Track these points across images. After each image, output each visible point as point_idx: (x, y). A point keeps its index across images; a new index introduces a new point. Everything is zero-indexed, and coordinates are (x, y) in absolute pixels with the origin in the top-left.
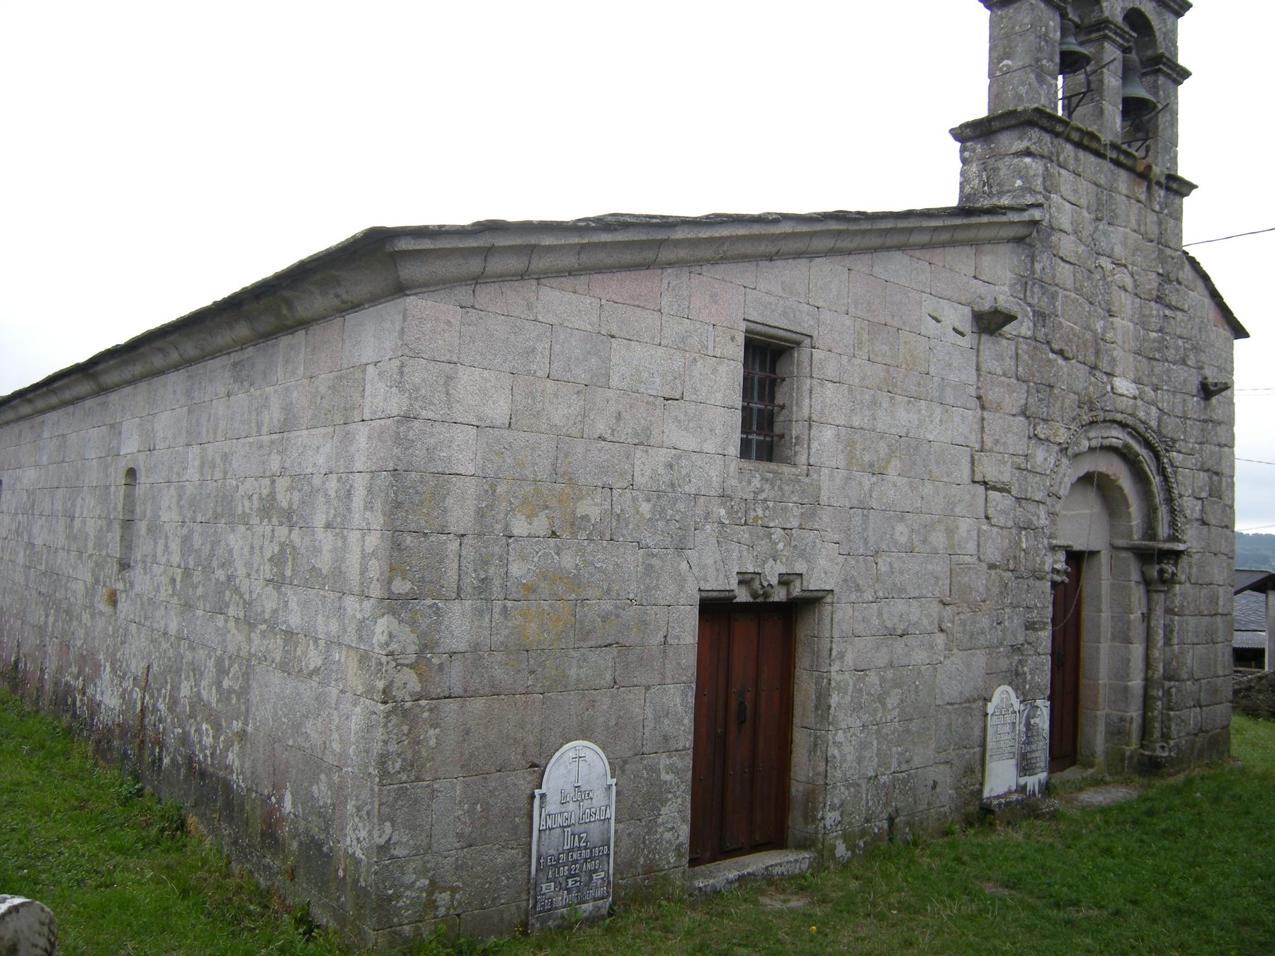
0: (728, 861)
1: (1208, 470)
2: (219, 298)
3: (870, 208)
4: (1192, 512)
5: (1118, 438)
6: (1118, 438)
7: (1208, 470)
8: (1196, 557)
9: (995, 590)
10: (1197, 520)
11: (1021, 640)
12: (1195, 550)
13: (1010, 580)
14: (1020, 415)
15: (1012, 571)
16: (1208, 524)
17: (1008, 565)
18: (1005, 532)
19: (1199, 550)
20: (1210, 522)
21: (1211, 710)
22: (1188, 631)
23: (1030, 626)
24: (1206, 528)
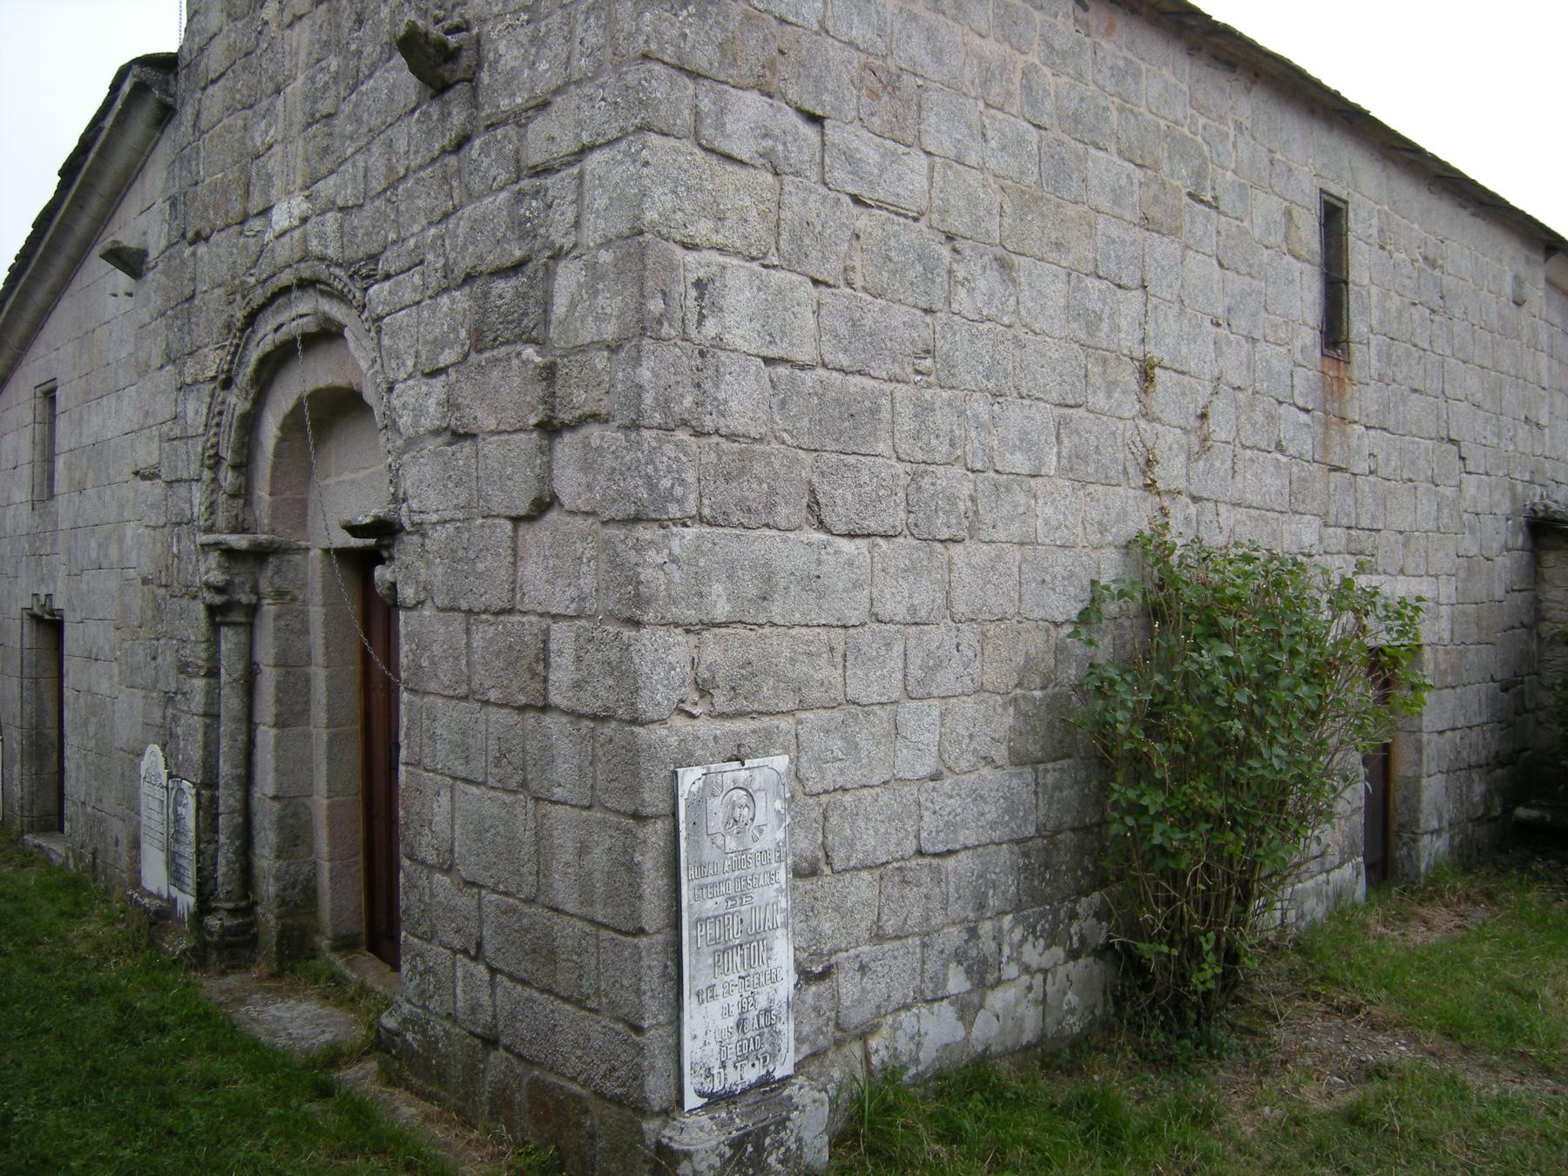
0: (1352, 224)
1: (469, 278)
2: (1344, 94)
3: (19, 243)
4: (416, 418)
5: (301, 316)
6: (301, 316)
7: (469, 278)
8: (440, 534)
9: (150, 613)
10: (437, 432)
11: (173, 687)
12: (434, 518)
13: (164, 599)
14: (167, 364)
15: (166, 586)
16: (473, 436)
17: (160, 578)
18: (158, 533)
19: (448, 515)
20: (473, 429)
21: (530, 1000)
22: (433, 737)
23: (183, 668)
24: (467, 447)
